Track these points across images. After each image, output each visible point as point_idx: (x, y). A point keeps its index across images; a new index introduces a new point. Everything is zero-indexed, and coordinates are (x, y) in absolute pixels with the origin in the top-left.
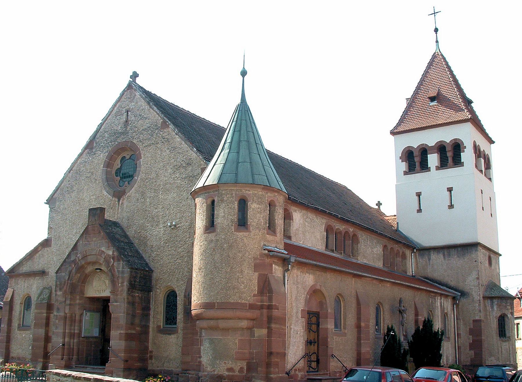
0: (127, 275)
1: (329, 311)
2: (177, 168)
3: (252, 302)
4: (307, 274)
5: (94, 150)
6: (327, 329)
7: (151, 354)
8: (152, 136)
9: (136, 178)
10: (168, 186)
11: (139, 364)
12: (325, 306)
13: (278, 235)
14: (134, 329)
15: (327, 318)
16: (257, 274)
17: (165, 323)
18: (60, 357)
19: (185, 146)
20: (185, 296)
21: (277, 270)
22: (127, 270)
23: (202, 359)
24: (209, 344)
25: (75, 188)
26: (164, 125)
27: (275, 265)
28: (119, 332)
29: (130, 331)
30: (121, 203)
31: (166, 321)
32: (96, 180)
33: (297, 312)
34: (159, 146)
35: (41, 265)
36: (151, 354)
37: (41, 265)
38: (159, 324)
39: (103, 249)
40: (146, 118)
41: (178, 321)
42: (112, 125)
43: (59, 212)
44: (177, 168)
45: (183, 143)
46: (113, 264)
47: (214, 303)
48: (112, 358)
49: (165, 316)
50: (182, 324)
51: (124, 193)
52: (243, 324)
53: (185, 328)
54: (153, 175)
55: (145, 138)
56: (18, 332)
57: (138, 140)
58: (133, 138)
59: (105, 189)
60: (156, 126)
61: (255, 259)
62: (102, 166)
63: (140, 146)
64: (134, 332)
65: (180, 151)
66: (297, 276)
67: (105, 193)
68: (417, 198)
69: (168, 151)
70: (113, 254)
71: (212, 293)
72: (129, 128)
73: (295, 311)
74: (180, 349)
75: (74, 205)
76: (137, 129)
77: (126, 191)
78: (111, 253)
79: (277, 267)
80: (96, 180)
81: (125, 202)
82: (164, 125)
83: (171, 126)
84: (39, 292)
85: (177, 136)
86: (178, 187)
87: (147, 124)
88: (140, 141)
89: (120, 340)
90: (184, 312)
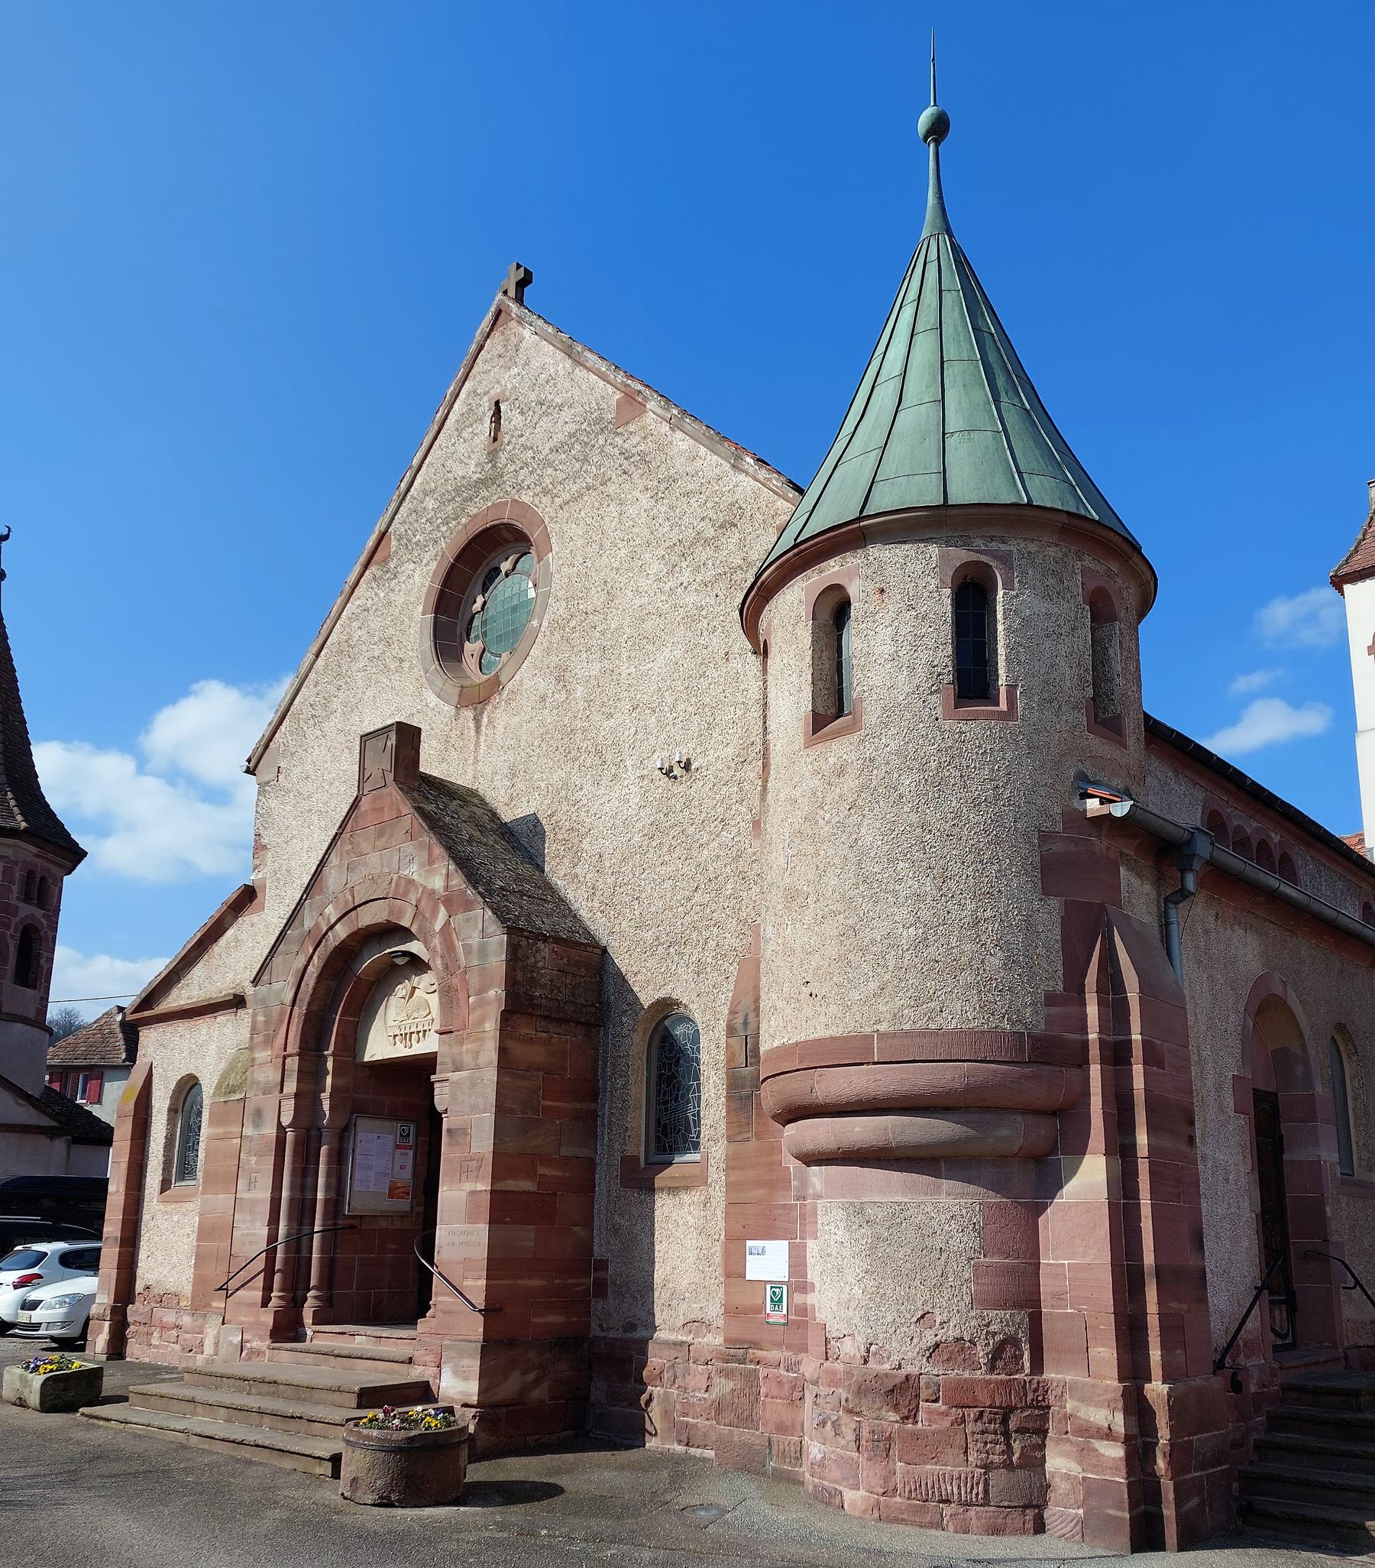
0: (497, 961)
1: (1319, 1089)
2: (684, 549)
3: (1040, 1028)
4: (1240, 931)
5: (392, 565)
6: (1316, 1166)
7: (601, 1274)
8: (586, 460)
9: (535, 623)
10: (649, 625)
11: (557, 1319)
12: (1299, 1070)
13: (1131, 741)
14: (531, 1174)
15: (1314, 1119)
16: (1055, 903)
17: (652, 1146)
18: (258, 1295)
19: (711, 462)
20: (731, 1031)
21: (1137, 892)
22: (498, 940)
23: (811, 1299)
24: (848, 1228)
25: (336, 704)
26: (631, 406)
27: (1130, 869)
28: (469, 1186)
29: (510, 1185)
30: (485, 720)
31: (658, 1140)
32: (401, 660)
33: (1219, 1088)
34: (612, 488)
35: (230, 975)
36: (601, 1274)
37: (230, 975)
38: (630, 1150)
39: (413, 871)
40: (561, 407)
41: (705, 1132)
42: (449, 463)
43: (288, 791)
44: (684, 549)
45: (703, 450)
46: (447, 924)
47: (868, 1038)
48: (441, 1298)
49: (653, 1116)
50: (723, 1144)
51: (495, 685)
52: (1005, 1132)
53: (732, 1164)
54: (597, 599)
55: (561, 476)
56: (161, 1206)
57: (539, 489)
58: (519, 487)
59: (431, 683)
60: (599, 420)
61: (1045, 837)
62: (420, 608)
63: (545, 508)
64: (526, 1185)
65: (690, 487)
66: (1206, 932)
67: (432, 699)
68: (405, 1357)
69: (645, 500)
70: (447, 888)
71: (855, 995)
72: (503, 458)
73: (1210, 1083)
74: (718, 1249)
75: (334, 759)
76: (530, 453)
77: (503, 678)
78: (437, 883)
79: (1135, 882)
80: (401, 660)
81: (501, 716)
82: (631, 406)
83: (653, 404)
84: (223, 1065)
85: (679, 435)
86: (690, 620)
87: (564, 424)
88: (546, 492)
89: (471, 1219)
90: (729, 1098)
